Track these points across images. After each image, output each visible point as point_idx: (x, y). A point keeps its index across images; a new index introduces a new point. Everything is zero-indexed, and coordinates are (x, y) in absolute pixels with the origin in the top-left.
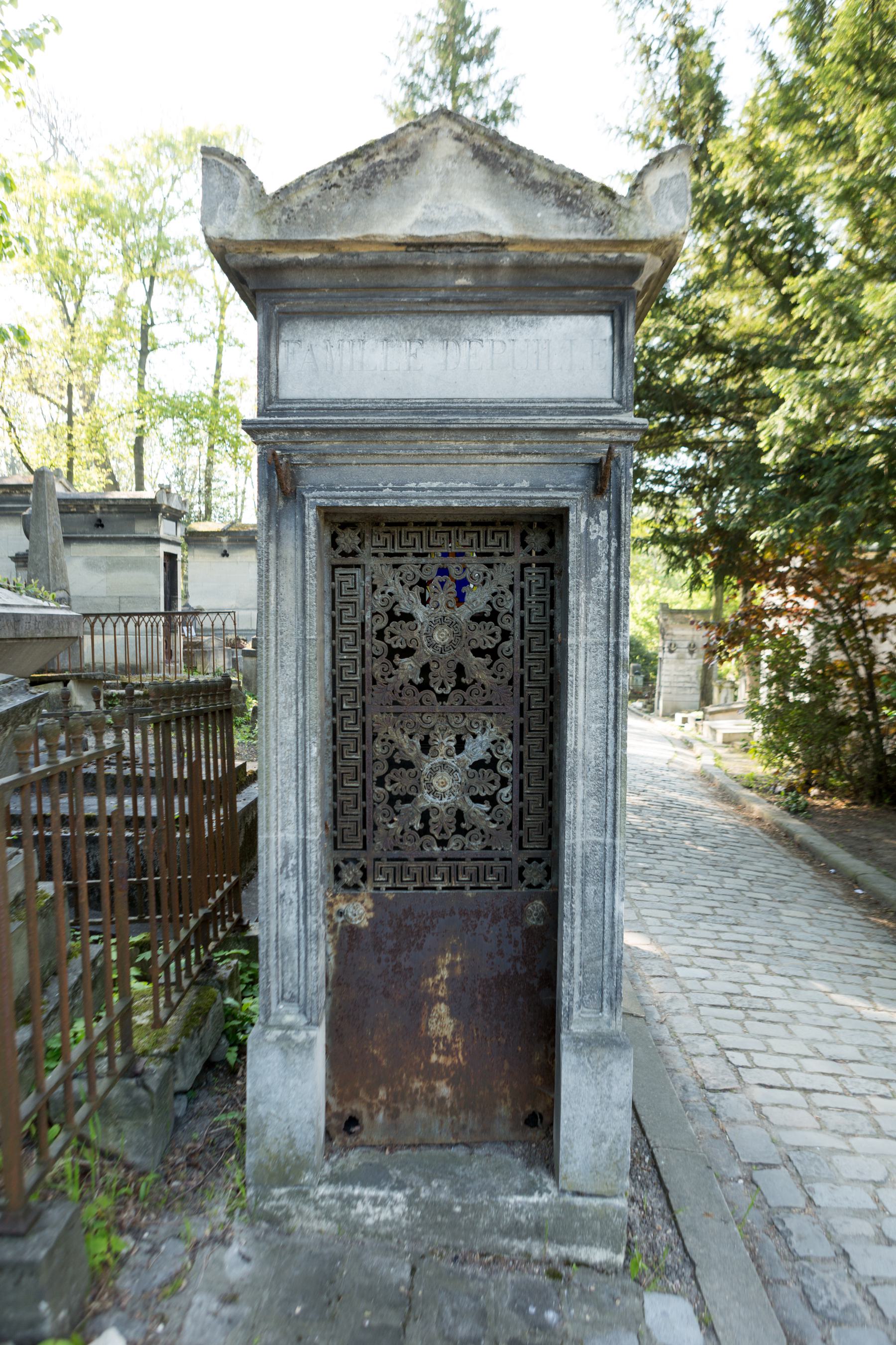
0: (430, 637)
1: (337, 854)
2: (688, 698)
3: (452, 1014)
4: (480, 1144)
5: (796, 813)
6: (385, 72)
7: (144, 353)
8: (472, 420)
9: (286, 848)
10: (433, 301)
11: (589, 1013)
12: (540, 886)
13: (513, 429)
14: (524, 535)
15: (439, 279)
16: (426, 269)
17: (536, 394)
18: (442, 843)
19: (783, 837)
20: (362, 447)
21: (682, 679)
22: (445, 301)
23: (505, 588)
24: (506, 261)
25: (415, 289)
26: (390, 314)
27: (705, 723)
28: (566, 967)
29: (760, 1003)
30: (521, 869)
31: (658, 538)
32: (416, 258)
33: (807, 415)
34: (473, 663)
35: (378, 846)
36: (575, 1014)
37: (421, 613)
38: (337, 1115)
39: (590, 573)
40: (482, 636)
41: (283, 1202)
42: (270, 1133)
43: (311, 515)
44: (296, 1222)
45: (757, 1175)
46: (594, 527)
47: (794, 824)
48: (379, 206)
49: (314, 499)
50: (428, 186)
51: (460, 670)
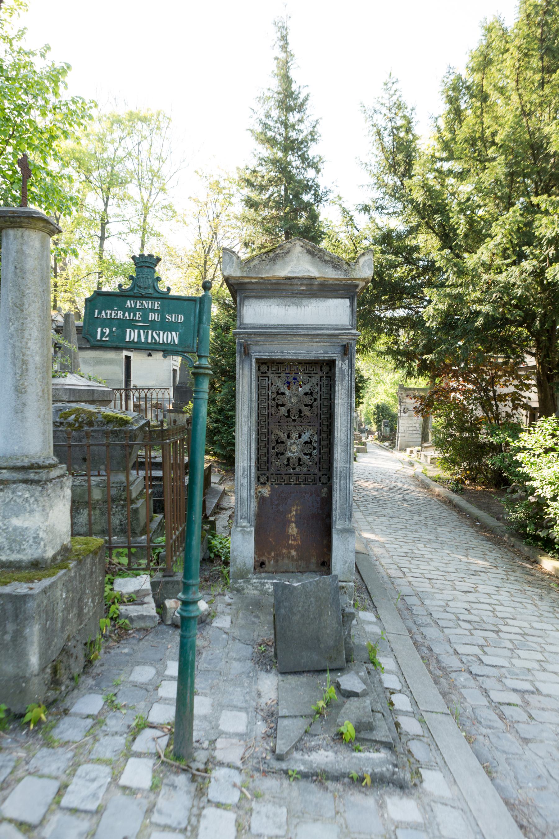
0: (290, 400)
1: (259, 472)
2: (415, 440)
3: (296, 527)
4: (305, 572)
5: (456, 492)
6: (251, 117)
7: (102, 238)
8: (305, 331)
9: (244, 468)
10: (293, 294)
11: (342, 522)
12: (326, 483)
13: (318, 335)
14: (321, 367)
15: (295, 287)
16: (291, 285)
17: (325, 323)
18: (294, 469)
19: (449, 503)
20: (270, 340)
21: (411, 429)
22: (297, 294)
23: (315, 384)
24: (316, 283)
25: (288, 290)
26: (279, 297)
27: (422, 453)
28: (334, 507)
29: (419, 556)
30: (320, 478)
31: (389, 351)
32: (288, 281)
33: (442, 307)
34: (304, 409)
35: (272, 470)
36: (337, 522)
37: (287, 392)
38: (257, 561)
39: (343, 380)
40: (307, 400)
41: (242, 584)
42: (238, 561)
43: (254, 361)
44: (246, 591)
45: (405, 598)
46: (344, 365)
47: (456, 498)
48: (277, 267)
49: (255, 356)
50: (293, 261)
51: (300, 411)
